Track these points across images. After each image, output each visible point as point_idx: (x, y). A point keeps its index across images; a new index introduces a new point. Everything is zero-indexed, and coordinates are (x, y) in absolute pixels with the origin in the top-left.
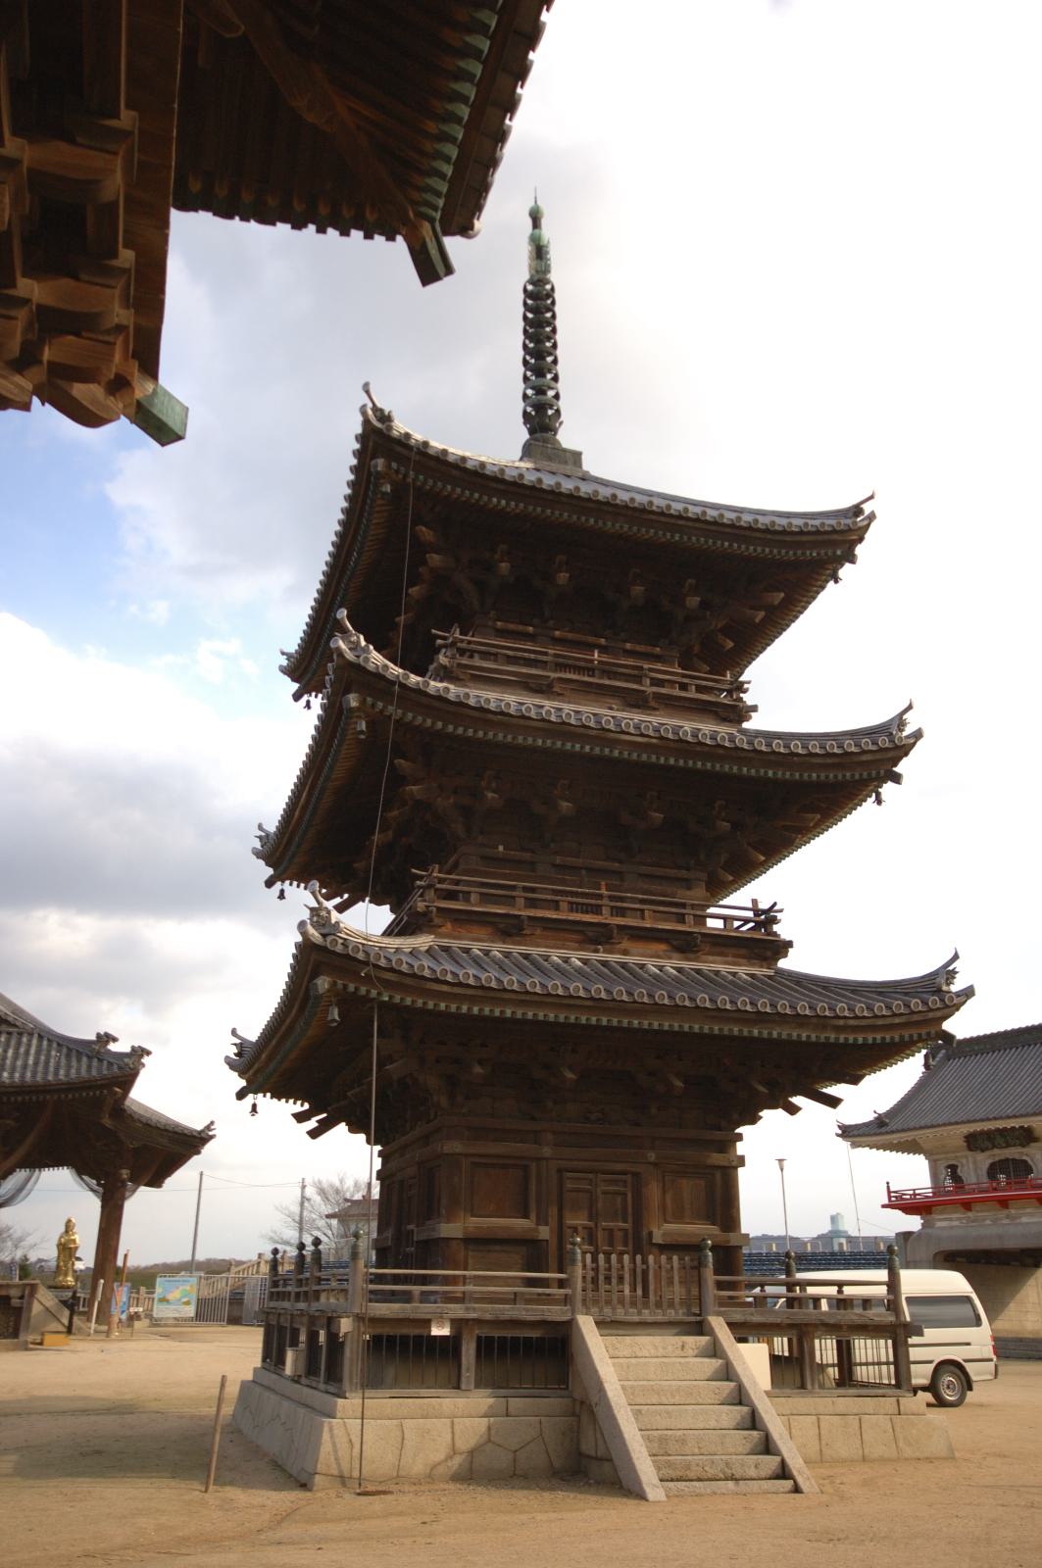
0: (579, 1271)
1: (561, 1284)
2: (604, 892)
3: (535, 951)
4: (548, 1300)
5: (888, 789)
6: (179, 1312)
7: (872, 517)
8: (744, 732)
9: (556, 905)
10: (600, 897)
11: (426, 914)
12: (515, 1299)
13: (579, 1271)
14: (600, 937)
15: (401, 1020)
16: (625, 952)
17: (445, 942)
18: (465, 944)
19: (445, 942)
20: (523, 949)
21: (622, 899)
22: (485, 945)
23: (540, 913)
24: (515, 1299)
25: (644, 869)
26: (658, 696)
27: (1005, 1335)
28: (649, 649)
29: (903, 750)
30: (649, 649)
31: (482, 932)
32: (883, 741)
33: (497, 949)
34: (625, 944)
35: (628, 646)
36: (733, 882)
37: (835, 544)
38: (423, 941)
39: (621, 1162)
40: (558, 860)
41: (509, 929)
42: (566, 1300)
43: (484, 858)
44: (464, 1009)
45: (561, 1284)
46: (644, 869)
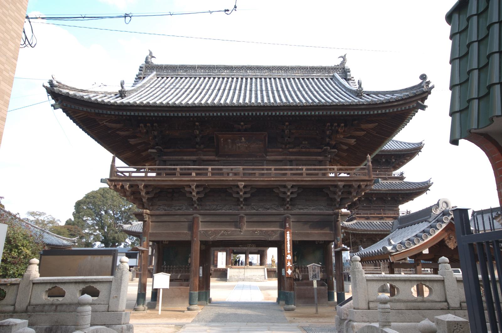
0: (382, 267)
1: (380, 268)
2: (382, 211)
3: (372, 221)
4: (378, 270)
5: (428, 192)
6: (310, 271)
7: (424, 144)
8: (403, 182)
9: (374, 214)
10: (381, 212)
11: (355, 217)
12: (373, 270)
13: (382, 267)
14: (381, 218)
15: (353, 234)
16: (386, 220)
17: (358, 221)
18: (361, 221)
19: (358, 221)
20: (370, 221)
21: (385, 212)
22: (364, 221)
23: (372, 215)
24: (373, 270)
25: (388, 205)
26: (388, 178)
27: (158, 294)
28: (387, 167)
29: (430, 186)
30: (387, 167)
31: (363, 219)
32: (426, 185)
33: (366, 222)
34: (386, 219)
35: (383, 167)
36: (409, 159)
37: (418, 149)
38: (355, 222)
39: (405, 322)
40: (374, 205)
41: (367, 218)
42: (380, 271)
43: (363, 206)
44: (285, 113)
45: (380, 268)
46: (388, 205)
